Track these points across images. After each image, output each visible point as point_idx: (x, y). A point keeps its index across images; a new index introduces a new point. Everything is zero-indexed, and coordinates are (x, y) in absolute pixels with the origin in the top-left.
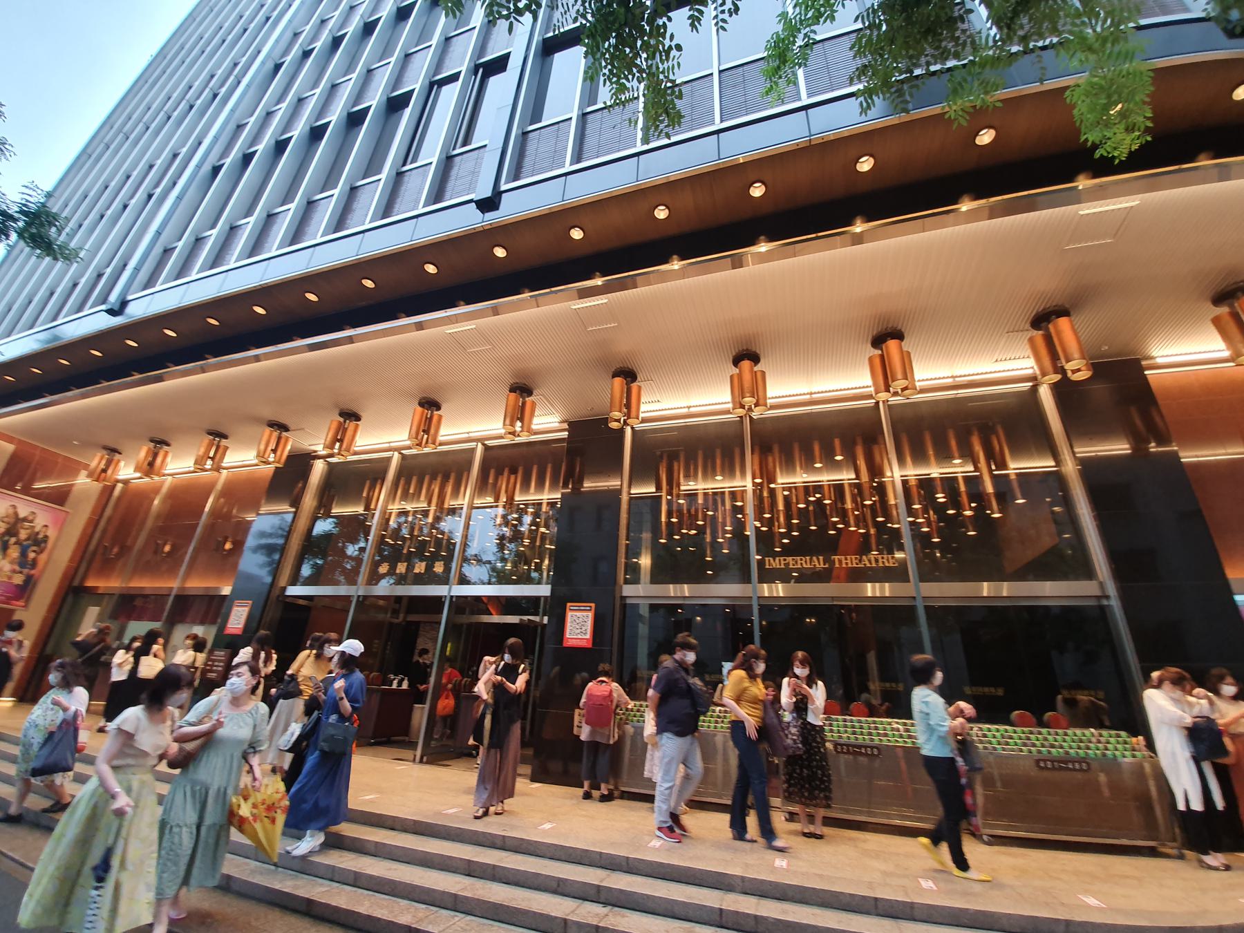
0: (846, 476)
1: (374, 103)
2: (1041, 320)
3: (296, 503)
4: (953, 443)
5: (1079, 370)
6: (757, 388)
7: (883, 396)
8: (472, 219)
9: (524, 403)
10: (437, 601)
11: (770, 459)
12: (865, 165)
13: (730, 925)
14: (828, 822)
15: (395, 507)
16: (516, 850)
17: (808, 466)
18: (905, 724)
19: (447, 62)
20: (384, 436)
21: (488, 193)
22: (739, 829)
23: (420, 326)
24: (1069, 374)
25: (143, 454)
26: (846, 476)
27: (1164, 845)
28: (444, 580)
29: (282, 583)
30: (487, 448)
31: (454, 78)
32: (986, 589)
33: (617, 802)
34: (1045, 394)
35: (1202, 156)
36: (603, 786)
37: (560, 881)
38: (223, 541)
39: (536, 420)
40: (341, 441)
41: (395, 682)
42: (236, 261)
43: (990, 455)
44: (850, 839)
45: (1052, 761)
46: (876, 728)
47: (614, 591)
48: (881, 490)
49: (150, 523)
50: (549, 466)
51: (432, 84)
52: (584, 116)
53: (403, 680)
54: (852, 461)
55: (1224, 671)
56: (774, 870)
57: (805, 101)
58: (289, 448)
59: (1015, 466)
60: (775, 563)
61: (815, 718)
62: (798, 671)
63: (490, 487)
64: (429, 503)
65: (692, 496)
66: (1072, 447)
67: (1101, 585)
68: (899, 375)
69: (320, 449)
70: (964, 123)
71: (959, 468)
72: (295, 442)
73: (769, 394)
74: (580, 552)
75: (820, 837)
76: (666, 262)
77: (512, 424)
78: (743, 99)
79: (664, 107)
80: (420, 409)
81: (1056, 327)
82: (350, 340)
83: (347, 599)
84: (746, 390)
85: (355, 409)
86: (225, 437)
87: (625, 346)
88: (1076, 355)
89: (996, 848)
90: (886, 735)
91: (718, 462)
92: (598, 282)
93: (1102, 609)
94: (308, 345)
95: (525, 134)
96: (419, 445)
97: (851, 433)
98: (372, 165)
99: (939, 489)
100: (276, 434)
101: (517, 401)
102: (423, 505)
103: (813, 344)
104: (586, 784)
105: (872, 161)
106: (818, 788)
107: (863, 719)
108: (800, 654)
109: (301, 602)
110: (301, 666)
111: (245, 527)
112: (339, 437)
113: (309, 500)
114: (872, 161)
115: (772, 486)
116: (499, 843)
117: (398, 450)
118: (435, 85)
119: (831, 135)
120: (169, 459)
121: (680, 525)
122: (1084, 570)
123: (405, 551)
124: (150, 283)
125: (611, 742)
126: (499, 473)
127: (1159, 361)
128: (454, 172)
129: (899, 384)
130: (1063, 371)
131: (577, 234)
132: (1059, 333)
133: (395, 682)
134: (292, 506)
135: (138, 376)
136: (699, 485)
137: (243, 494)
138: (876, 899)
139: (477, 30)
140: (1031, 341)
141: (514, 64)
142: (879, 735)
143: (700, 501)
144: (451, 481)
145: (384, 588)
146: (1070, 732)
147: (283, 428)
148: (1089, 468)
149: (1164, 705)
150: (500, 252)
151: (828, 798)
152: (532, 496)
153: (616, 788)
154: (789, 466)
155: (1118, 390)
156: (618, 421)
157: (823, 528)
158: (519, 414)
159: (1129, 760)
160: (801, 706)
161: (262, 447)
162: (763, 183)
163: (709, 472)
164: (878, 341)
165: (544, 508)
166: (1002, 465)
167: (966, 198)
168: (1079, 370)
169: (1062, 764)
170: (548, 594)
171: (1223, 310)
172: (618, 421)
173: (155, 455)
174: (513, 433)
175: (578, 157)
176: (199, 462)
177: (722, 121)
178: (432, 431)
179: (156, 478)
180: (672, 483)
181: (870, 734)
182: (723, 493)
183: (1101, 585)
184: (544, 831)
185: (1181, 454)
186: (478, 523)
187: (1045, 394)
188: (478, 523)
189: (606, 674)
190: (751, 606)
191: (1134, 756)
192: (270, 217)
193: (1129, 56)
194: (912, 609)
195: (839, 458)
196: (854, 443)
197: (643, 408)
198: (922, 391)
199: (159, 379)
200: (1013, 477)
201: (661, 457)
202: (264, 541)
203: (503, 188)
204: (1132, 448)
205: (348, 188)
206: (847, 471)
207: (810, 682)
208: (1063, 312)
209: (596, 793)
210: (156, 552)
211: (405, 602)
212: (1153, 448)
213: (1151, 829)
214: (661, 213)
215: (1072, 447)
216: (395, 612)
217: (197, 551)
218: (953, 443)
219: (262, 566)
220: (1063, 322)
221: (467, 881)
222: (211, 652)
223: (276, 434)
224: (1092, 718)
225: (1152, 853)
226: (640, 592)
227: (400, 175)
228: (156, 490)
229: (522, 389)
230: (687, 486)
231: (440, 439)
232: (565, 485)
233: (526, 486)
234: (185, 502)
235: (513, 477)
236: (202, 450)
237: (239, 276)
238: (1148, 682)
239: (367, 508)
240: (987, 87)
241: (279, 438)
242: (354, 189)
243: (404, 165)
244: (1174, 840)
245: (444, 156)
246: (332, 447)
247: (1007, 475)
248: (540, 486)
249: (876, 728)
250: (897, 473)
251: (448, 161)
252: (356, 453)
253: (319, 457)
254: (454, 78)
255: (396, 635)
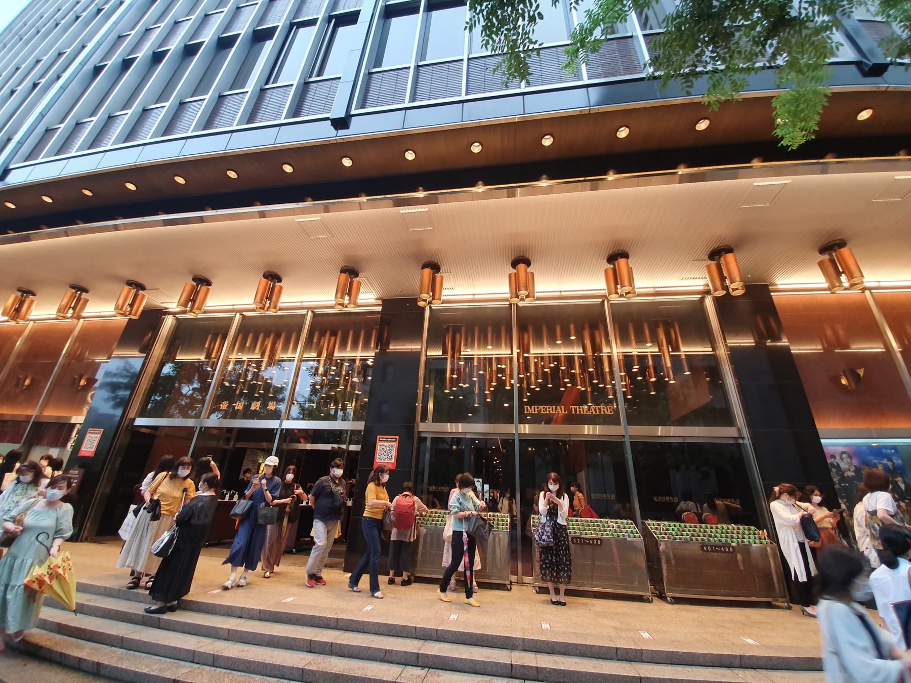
0: (577, 351)
1: (207, 40)
2: (716, 254)
3: (146, 349)
4: (647, 332)
5: (737, 289)
6: (529, 284)
7: (515, 300)
8: (325, 133)
9: (351, 283)
10: (270, 433)
11: (526, 336)
12: (623, 133)
13: (518, 676)
14: (569, 593)
15: (233, 357)
16: (347, 629)
17: (552, 341)
18: (617, 523)
19: (305, 10)
20: (231, 299)
21: (342, 115)
22: (354, 582)
23: (262, 215)
24: (731, 291)
25: (10, 301)
26: (577, 351)
27: (777, 601)
28: (276, 415)
29: (132, 415)
30: (315, 315)
31: (312, 23)
32: (660, 431)
33: (414, 585)
34: (709, 302)
35: (829, 156)
36: (405, 574)
37: (386, 652)
38: (76, 381)
39: (361, 296)
40: (194, 301)
41: (228, 496)
42: (79, 150)
43: (669, 342)
44: (583, 604)
45: (711, 546)
46: (598, 526)
47: (413, 427)
48: (599, 361)
49: (12, 360)
50: (351, 333)
51: (292, 25)
52: (418, 67)
53: (234, 494)
54: (655, 340)
55: (814, 487)
56: (543, 631)
57: (464, 97)
58: (144, 304)
59: (685, 350)
60: (531, 410)
61: (561, 521)
62: (551, 487)
63: (314, 346)
64: (263, 355)
65: (469, 359)
66: (725, 339)
67: (739, 430)
68: (626, 283)
69: (173, 305)
70: (716, 110)
71: (650, 349)
72: (150, 299)
73: (536, 289)
74: (389, 397)
75: (564, 604)
76: (474, 186)
77: (342, 298)
78: (540, 73)
79: (518, 66)
80: (265, 280)
81: (725, 260)
82: (201, 220)
83: (191, 430)
84: (522, 285)
85: (84, 285)
86: (87, 291)
87: (435, 245)
88: (738, 279)
89: (676, 606)
90: (605, 531)
91: (489, 336)
92: (421, 194)
93: (738, 446)
94: (163, 220)
95: (370, 74)
96: (263, 308)
97: (585, 321)
98: (200, 86)
99: (636, 362)
100: (134, 291)
101: (346, 280)
102: (256, 356)
103: (568, 257)
104: (391, 572)
105: (627, 130)
106: (563, 570)
107: (589, 519)
108: (553, 475)
109: (143, 430)
110: (159, 484)
111: (96, 367)
112: (192, 298)
113: (158, 349)
114: (627, 130)
115: (526, 355)
116: (333, 624)
117: (240, 311)
118: (294, 26)
119: (540, 116)
120: (33, 307)
121: (458, 380)
122: (726, 418)
123: (238, 392)
124: (33, 154)
125: (412, 540)
126: (322, 334)
127: (780, 287)
128: (310, 95)
129: (523, 293)
130: (726, 288)
131: (410, 156)
132: (727, 264)
133: (228, 496)
134: (141, 351)
135: (12, 234)
136: (477, 352)
137: (98, 340)
138: (617, 649)
139: (258, 6)
140: (708, 267)
141: (364, 19)
142: (600, 530)
143: (476, 363)
144: (282, 339)
145: (214, 421)
146: (719, 526)
147: (140, 287)
148: (736, 354)
149: (785, 512)
150: (347, 162)
151: (569, 577)
152: (348, 354)
153: (412, 574)
154: (539, 341)
155: (753, 306)
156: (425, 301)
157: (557, 386)
158: (348, 290)
159: (758, 545)
160: (553, 512)
161: (121, 302)
162: (552, 136)
163: (484, 343)
164: (612, 259)
165: (358, 363)
166: (677, 349)
167: (682, 166)
168: (737, 289)
169: (718, 548)
170: (363, 428)
171: (826, 257)
172: (425, 301)
173: (22, 303)
174: (342, 305)
175: (413, 98)
176: (62, 310)
177: (467, 94)
178: (274, 299)
179: (22, 322)
180: (455, 349)
181: (595, 530)
182: (491, 359)
183: (739, 430)
184: (368, 613)
185: (791, 348)
186: (294, 372)
187: (709, 302)
188: (294, 372)
189: (409, 490)
190: (514, 440)
191: (761, 543)
192: (111, 118)
193: (819, 80)
194: (621, 444)
195: (573, 338)
196: (583, 328)
197: (444, 292)
198: (639, 295)
199: (27, 239)
200: (683, 357)
201: (447, 329)
202: (109, 380)
203: (353, 112)
204: (756, 342)
205: (107, 117)
206: (578, 347)
207: (559, 494)
208: (729, 250)
209: (398, 579)
210: (17, 385)
211: (235, 433)
212: (769, 343)
213: (769, 588)
214: (476, 149)
215: (725, 339)
216: (228, 440)
217: (54, 385)
218: (647, 332)
219: (106, 400)
220: (730, 257)
221: (310, 657)
222: (66, 471)
223: (134, 291)
224: (733, 518)
225: (769, 605)
226: (427, 427)
227: (263, 91)
228: (19, 333)
229: (351, 271)
230: (466, 352)
231: (280, 305)
232: (377, 348)
233: (343, 346)
234: (44, 345)
235: (333, 339)
236: (65, 301)
237: (114, 158)
238: (771, 496)
239: (208, 356)
240: (736, 87)
241: (136, 296)
242: (182, 104)
243: (267, 83)
244: (785, 597)
245: (302, 81)
246: (186, 306)
247: (680, 356)
248: (355, 346)
249: (598, 526)
250: (615, 350)
251: (305, 85)
252: (205, 312)
253: (170, 313)
254: (312, 23)
255: (232, 455)
